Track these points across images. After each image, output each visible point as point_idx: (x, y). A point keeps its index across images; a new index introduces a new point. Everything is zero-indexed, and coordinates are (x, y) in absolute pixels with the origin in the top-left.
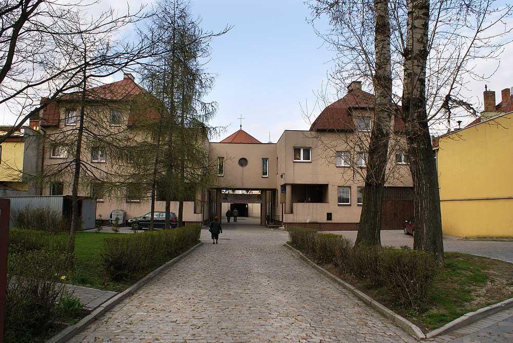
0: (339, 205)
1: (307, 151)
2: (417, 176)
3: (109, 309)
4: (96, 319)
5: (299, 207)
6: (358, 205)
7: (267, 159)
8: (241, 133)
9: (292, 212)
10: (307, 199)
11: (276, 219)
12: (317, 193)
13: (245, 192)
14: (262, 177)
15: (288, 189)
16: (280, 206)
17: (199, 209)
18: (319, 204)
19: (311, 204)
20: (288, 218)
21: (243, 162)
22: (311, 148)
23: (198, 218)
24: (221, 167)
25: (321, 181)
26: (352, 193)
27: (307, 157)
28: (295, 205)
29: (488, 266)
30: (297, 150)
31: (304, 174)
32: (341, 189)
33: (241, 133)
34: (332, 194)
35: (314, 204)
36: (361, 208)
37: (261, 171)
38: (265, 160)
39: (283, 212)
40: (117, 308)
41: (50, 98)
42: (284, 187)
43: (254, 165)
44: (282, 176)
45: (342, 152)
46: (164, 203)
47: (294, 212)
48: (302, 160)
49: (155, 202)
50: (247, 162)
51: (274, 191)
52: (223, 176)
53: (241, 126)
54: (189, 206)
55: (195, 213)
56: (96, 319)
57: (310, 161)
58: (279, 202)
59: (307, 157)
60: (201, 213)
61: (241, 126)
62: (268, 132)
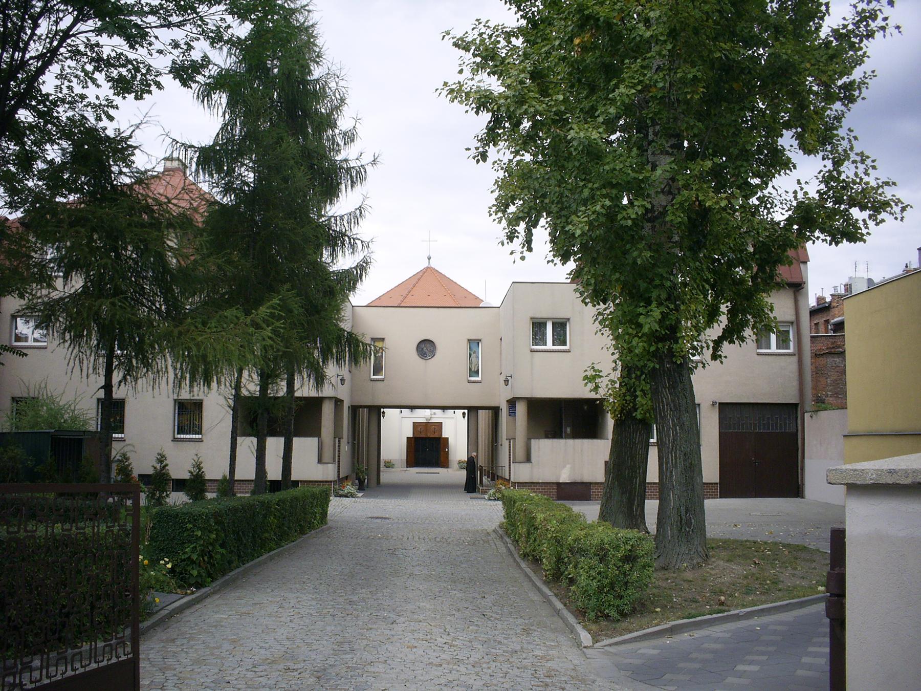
1: (560, 326)
2: (660, 414)
3: (181, 610)
4: (162, 621)
5: (544, 447)
7: (478, 342)
8: (429, 273)
9: (528, 459)
13: (344, 441)
14: (469, 382)
15: (521, 409)
16: (505, 444)
17: (328, 454)
18: (586, 442)
20: (521, 473)
21: (426, 348)
23: (327, 472)
27: (560, 339)
29: (669, 592)
30: (538, 326)
33: (429, 273)
35: (578, 442)
37: (466, 371)
38: (474, 343)
40: (188, 612)
41: (243, 30)
42: (512, 403)
43: (451, 352)
46: (282, 440)
48: (549, 345)
49: (240, 440)
51: (496, 411)
52: (383, 380)
53: (429, 258)
54: (305, 447)
55: (320, 461)
56: (162, 621)
57: (479, 379)
58: (504, 437)
59: (560, 339)
60: (334, 462)
61: (429, 258)
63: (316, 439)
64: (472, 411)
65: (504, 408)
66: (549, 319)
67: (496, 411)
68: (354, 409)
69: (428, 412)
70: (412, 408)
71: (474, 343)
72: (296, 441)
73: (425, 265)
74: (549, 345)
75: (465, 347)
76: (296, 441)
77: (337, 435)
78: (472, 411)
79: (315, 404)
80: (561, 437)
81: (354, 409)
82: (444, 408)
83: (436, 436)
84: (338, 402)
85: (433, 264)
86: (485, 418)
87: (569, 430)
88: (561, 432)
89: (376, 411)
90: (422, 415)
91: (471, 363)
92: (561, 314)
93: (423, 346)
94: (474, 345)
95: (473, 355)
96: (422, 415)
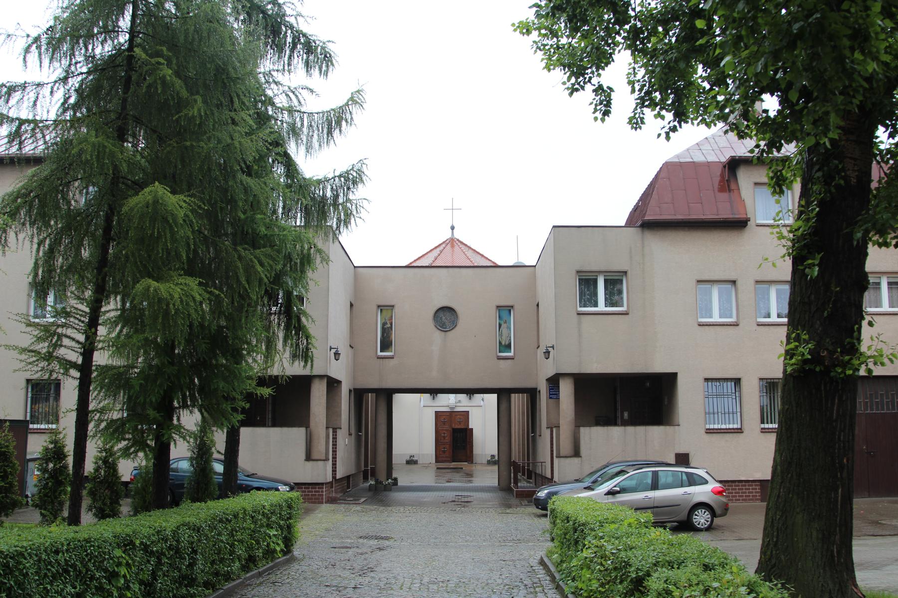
0: (709, 431)
1: (614, 284)
6: (764, 431)
7: (509, 309)
9: (577, 453)
10: (619, 414)
11: (539, 471)
12: (643, 398)
14: (499, 358)
15: (566, 389)
16: (546, 433)
19: (630, 429)
22: (625, 273)
24: (386, 332)
25: (659, 366)
26: (745, 410)
28: (584, 432)
30: (587, 283)
31: (608, 348)
32: (713, 387)
34: (689, 398)
35: (641, 429)
36: (772, 439)
38: (504, 310)
39: (552, 451)
42: (554, 382)
44: (547, 354)
45: (322, 484)
47: (583, 451)
48: (601, 307)
50: (457, 316)
51: (532, 393)
52: (392, 358)
53: (453, 228)
55: (309, 458)
57: (511, 354)
61: (453, 228)
62: (514, 239)
63: (302, 430)
64: (504, 394)
65: (543, 388)
66: (600, 272)
67: (532, 393)
68: (359, 395)
69: (451, 399)
70: (434, 392)
71: (504, 310)
72: (246, 433)
73: (449, 236)
74: (601, 307)
75: (493, 313)
76: (246, 433)
77: (333, 427)
78: (504, 394)
79: (302, 384)
80: (615, 424)
81: (359, 395)
82: (471, 392)
83: (462, 426)
84: (333, 384)
85: (457, 235)
86: (520, 402)
87: (626, 415)
88: (616, 418)
89: (387, 395)
90: (448, 401)
91: (501, 335)
92: (617, 265)
93: (441, 314)
94: (504, 314)
95: (504, 326)
96: (448, 401)
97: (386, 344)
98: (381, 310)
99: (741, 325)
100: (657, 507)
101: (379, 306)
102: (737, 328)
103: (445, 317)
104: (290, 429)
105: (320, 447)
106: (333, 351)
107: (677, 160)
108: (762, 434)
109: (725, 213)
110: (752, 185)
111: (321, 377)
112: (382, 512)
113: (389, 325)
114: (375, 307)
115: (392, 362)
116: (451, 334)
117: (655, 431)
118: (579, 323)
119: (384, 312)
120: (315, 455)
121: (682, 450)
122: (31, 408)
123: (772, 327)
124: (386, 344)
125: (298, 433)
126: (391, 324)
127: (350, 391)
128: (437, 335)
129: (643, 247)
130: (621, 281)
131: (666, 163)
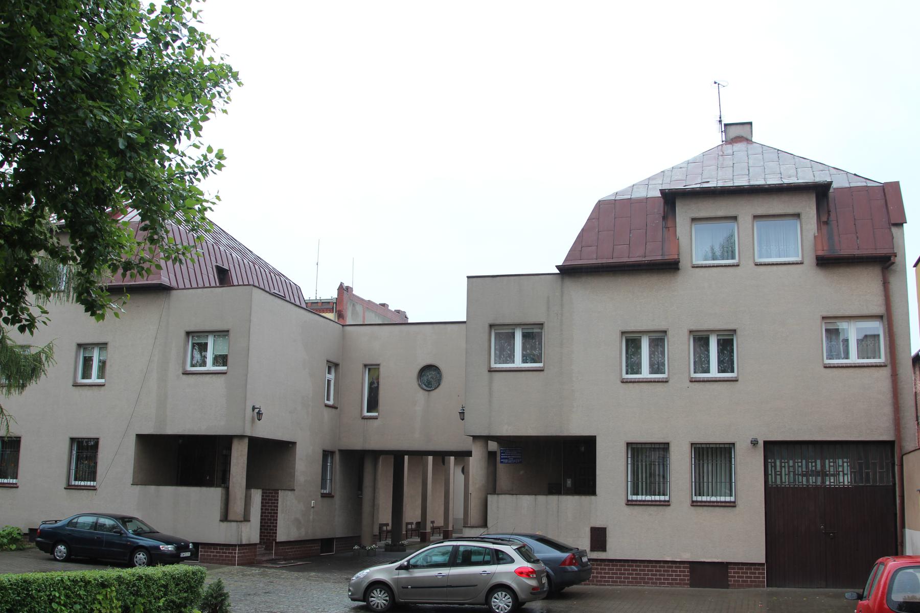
1: (533, 335)
25: (576, 428)
31: (524, 409)
34: (612, 467)
45: (235, 545)
48: (518, 363)
66: (712, 331)
74: (714, 373)
97: (373, 404)
98: (369, 370)
99: (670, 382)
100: (451, 586)
101: (365, 366)
102: (666, 384)
103: (429, 376)
104: (208, 489)
105: (237, 507)
106: (257, 410)
107: (613, 198)
108: (693, 508)
109: (656, 256)
110: (689, 220)
111: (241, 437)
112: (298, 579)
113: (376, 385)
114: (361, 366)
115: (376, 422)
116: (434, 394)
117: (570, 503)
118: (491, 381)
119: (372, 371)
120: (230, 517)
121: (598, 524)
122: (77, 467)
123: (707, 384)
124: (373, 404)
125: (214, 494)
126: (378, 383)
127: (327, 454)
128: (421, 395)
129: (562, 296)
130: (663, 340)
131: (599, 201)
